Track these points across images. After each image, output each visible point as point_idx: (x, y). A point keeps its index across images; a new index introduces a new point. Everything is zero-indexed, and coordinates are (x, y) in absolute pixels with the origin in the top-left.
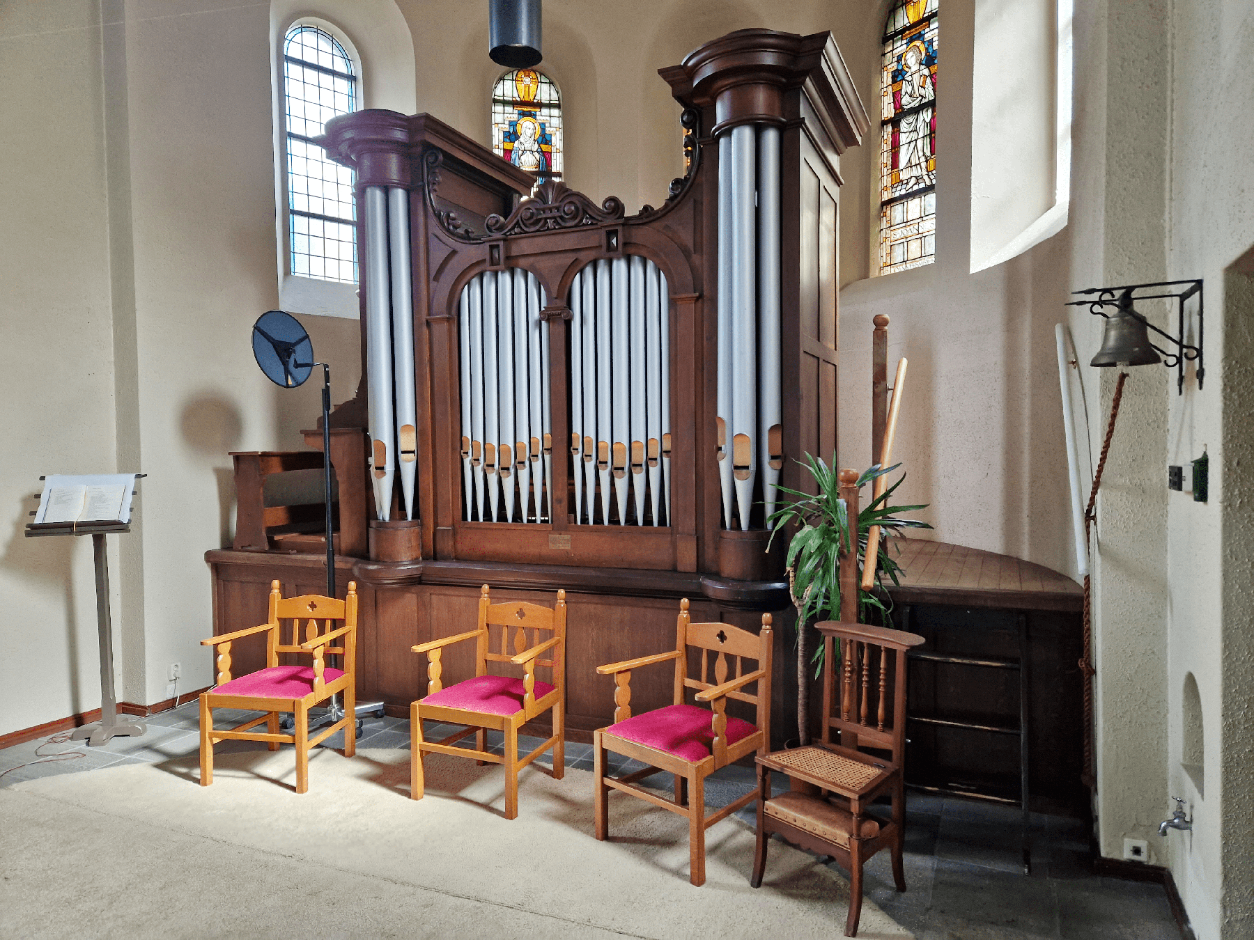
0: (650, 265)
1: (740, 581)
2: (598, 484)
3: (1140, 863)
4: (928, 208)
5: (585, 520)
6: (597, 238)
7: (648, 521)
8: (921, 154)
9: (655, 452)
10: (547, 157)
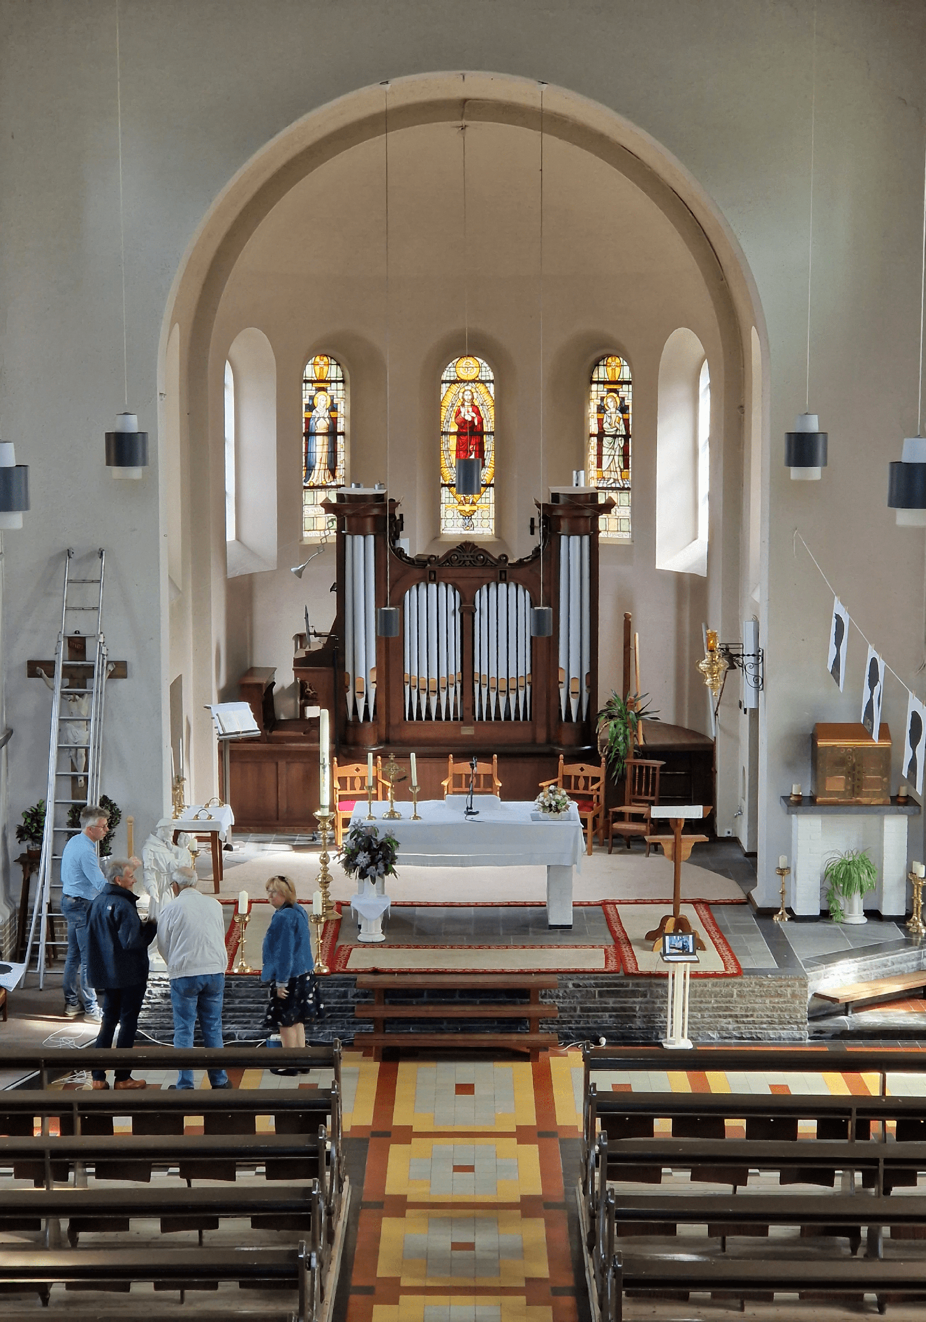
0: (450, 586)
1: (570, 746)
2: (489, 699)
3: (730, 837)
4: (622, 501)
5: (481, 718)
6: (491, 573)
7: (517, 718)
8: (617, 466)
9: (522, 682)
10: (334, 421)
